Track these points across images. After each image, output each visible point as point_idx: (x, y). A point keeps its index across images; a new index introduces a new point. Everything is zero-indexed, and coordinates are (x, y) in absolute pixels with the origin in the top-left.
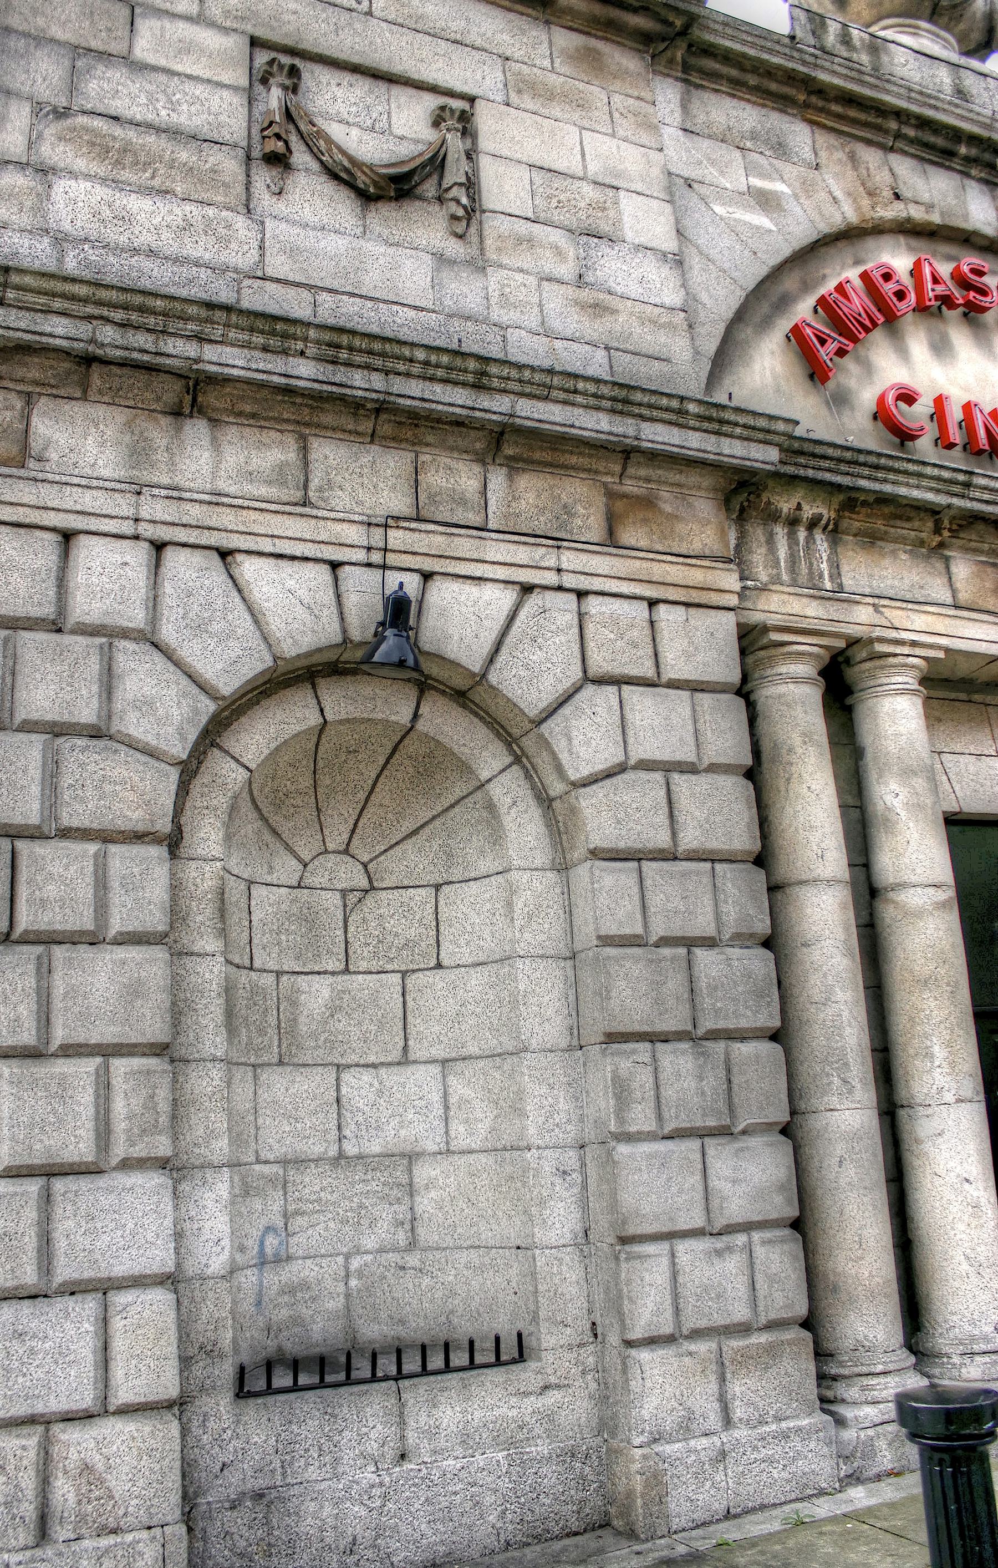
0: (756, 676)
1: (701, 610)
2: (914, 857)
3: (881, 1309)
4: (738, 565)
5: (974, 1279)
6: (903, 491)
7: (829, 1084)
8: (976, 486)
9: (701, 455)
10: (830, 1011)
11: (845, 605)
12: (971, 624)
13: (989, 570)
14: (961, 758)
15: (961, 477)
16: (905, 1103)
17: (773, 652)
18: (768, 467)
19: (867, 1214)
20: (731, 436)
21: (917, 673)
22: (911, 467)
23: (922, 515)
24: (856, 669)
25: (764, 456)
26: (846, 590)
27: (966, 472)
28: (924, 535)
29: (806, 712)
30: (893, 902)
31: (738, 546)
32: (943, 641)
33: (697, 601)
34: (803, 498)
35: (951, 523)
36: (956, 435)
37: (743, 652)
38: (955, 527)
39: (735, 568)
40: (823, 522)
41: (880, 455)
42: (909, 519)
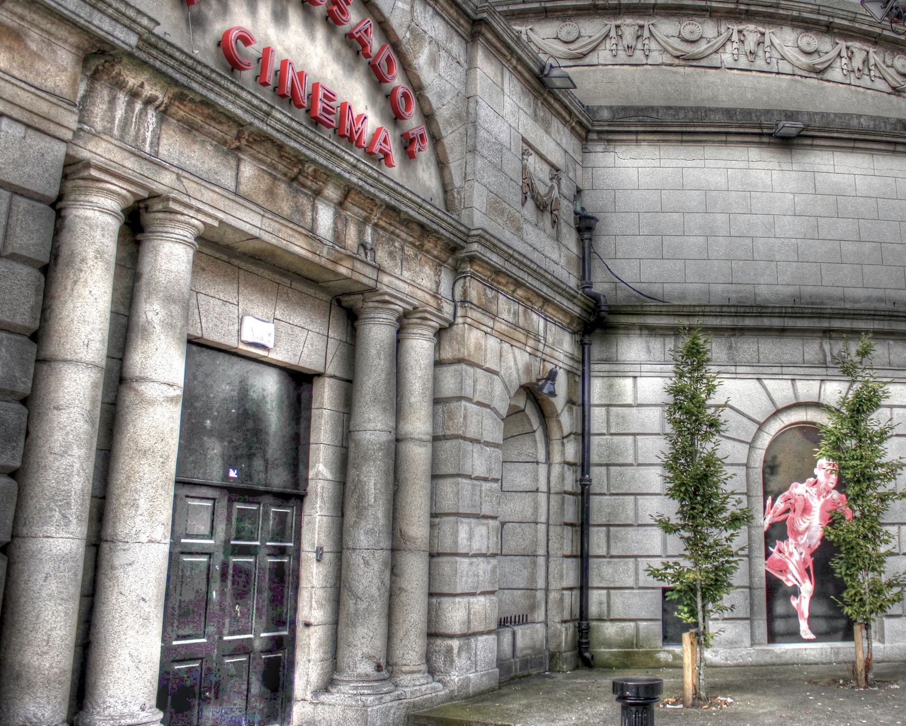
0: (72, 197)
1: (39, 134)
2: (158, 360)
3: (53, 693)
4: (81, 111)
5: (133, 672)
6: (222, 102)
7: (50, 517)
8: (273, 117)
9: (74, 17)
10: (65, 461)
11: (156, 168)
12: (243, 209)
13: (266, 177)
14: (212, 300)
15: (265, 107)
16: (109, 538)
17: (90, 184)
18: (126, 47)
19: (59, 619)
20: (103, 12)
21: (195, 231)
22: (232, 88)
23: (231, 123)
24: (152, 215)
25: (126, 38)
26: (160, 156)
27: (269, 105)
28: (228, 137)
29: (103, 236)
30: (136, 390)
31: (84, 97)
32: (221, 215)
33: (37, 126)
34: (147, 80)
35: (249, 136)
36: (270, 78)
37: (65, 177)
38: (251, 140)
39: (77, 111)
40: (157, 103)
41: (212, 71)
42: (220, 123)
